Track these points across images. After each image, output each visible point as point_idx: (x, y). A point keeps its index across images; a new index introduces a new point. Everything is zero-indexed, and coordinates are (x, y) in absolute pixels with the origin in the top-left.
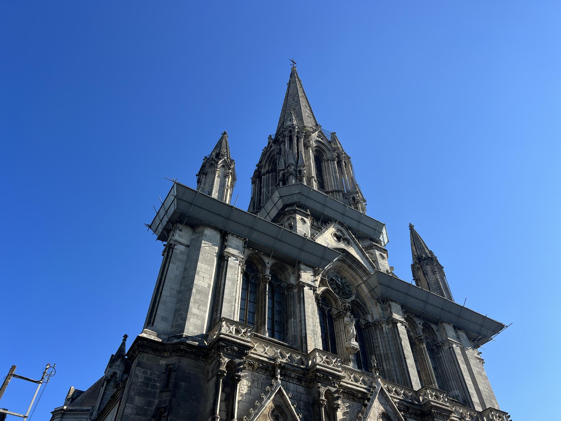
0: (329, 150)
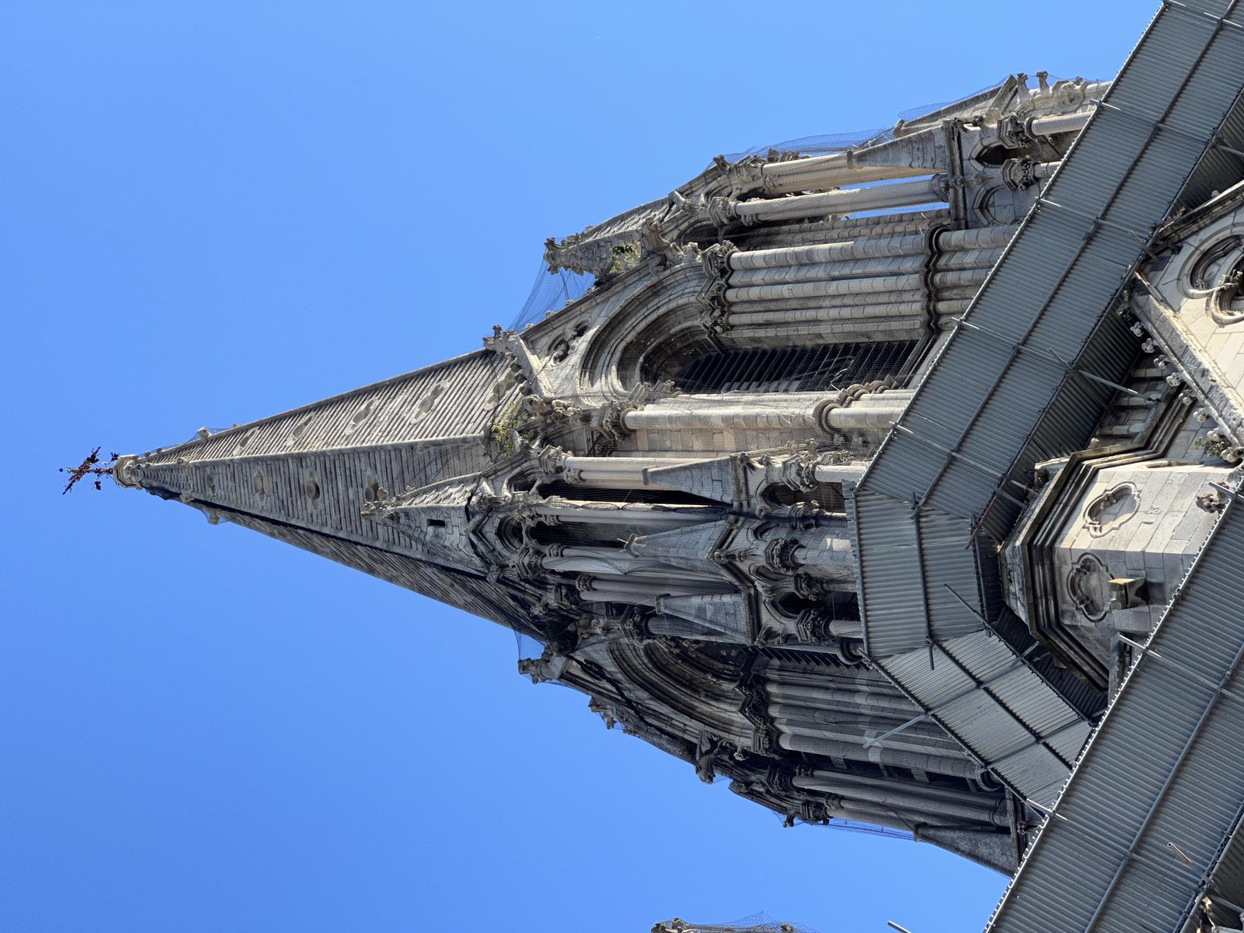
0: (655, 290)
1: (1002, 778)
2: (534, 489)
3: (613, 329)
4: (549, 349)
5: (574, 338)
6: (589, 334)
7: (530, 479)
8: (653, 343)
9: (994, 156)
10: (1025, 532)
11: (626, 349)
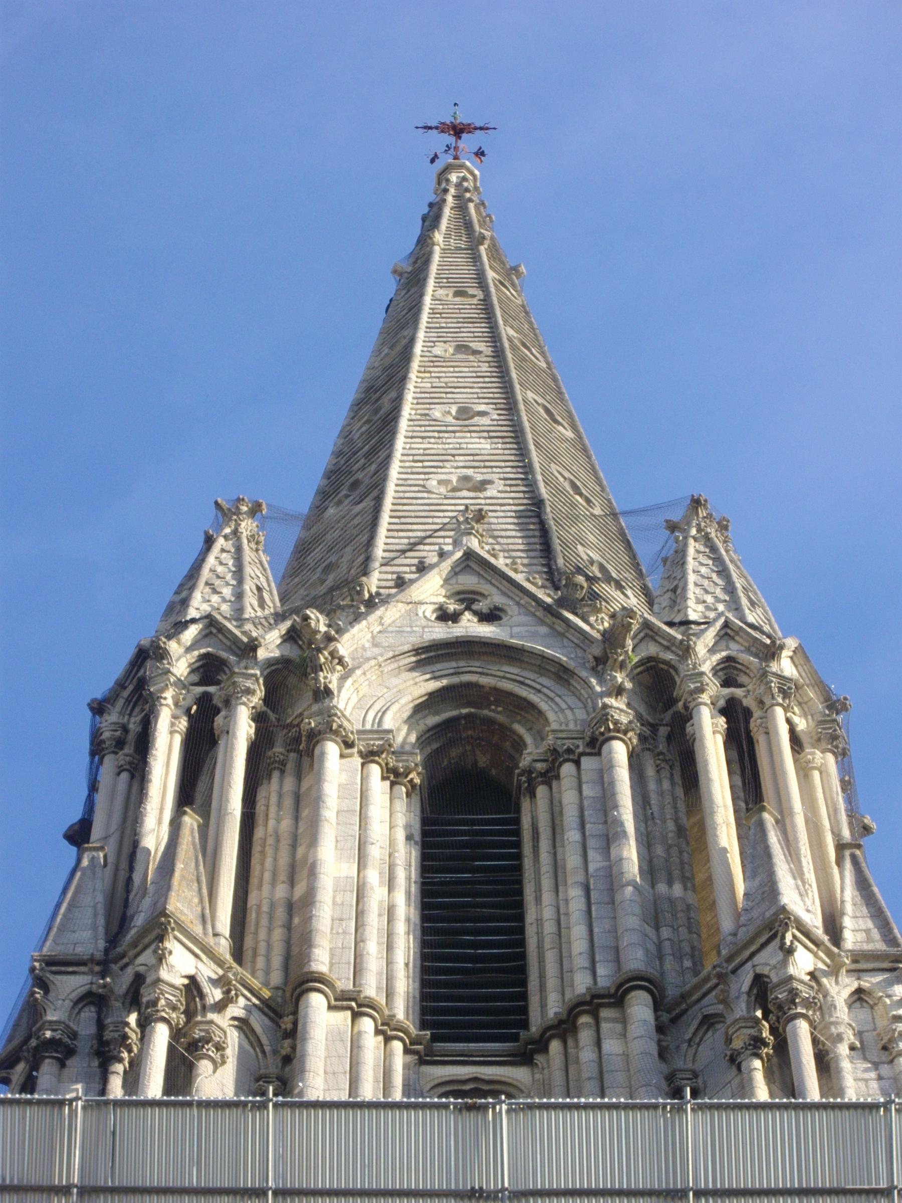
0: (562, 674)
1: (577, 1107)
2: (726, 691)
3: (492, 654)
4: (459, 593)
5: (475, 613)
6: (486, 631)
7: (742, 679)
8: (496, 713)
9: (761, 989)
10: (77, 1167)
11: (469, 685)
